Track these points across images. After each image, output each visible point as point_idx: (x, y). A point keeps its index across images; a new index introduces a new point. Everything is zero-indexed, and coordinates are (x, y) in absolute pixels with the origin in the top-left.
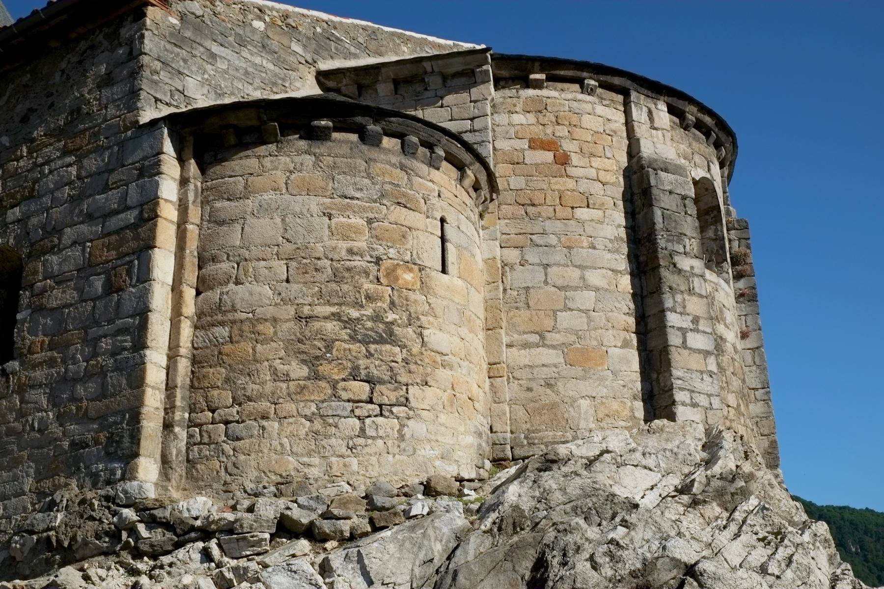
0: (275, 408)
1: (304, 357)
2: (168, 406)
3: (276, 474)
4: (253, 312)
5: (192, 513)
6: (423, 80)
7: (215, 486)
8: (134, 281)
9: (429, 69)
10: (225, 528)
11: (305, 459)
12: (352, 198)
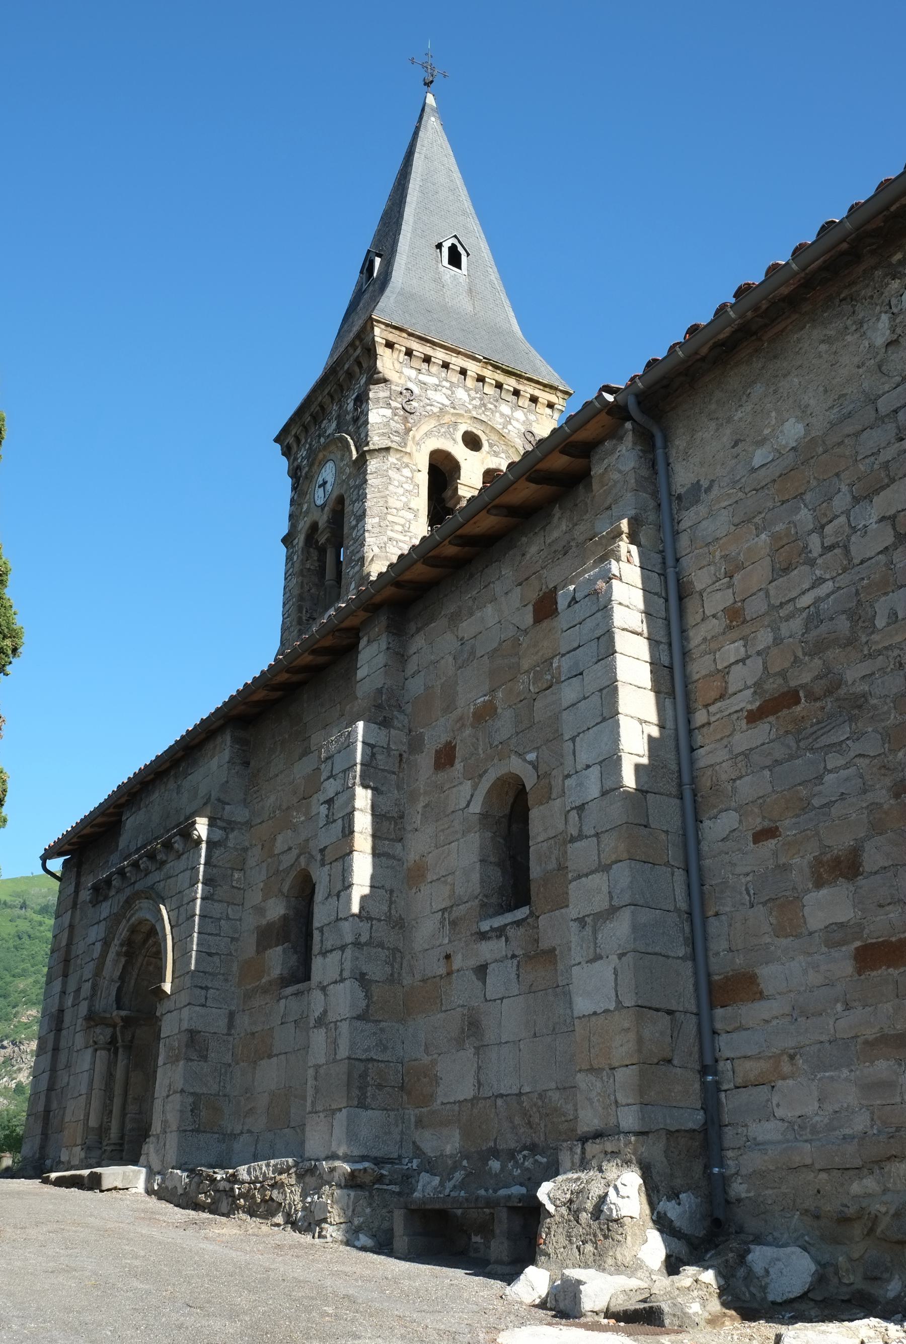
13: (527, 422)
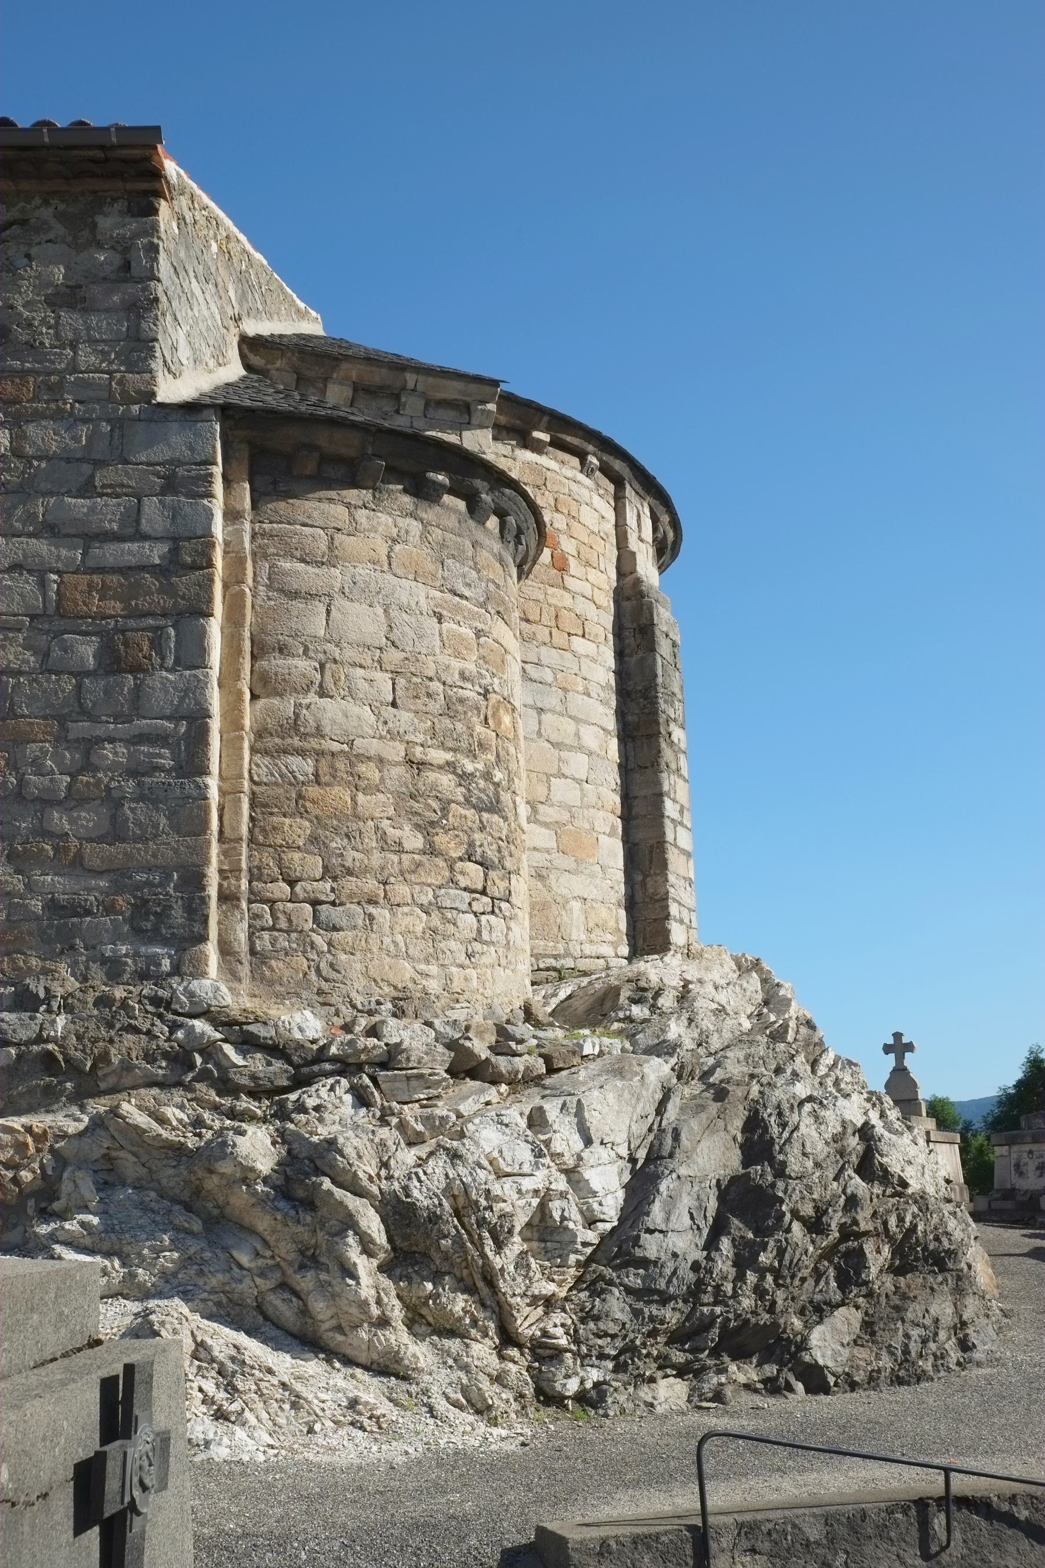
0: (385, 890)
1: (416, 819)
2: (226, 867)
3: (390, 984)
4: (351, 744)
5: (307, 1033)
6: (397, 397)
7: (305, 994)
8: (170, 662)
9: (411, 385)
10: (377, 1060)
11: (422, 967)
12: (461, 596)
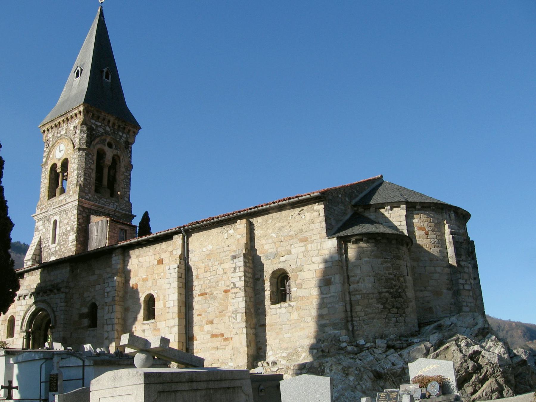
12: (387, 259)
13: (127, 138)
